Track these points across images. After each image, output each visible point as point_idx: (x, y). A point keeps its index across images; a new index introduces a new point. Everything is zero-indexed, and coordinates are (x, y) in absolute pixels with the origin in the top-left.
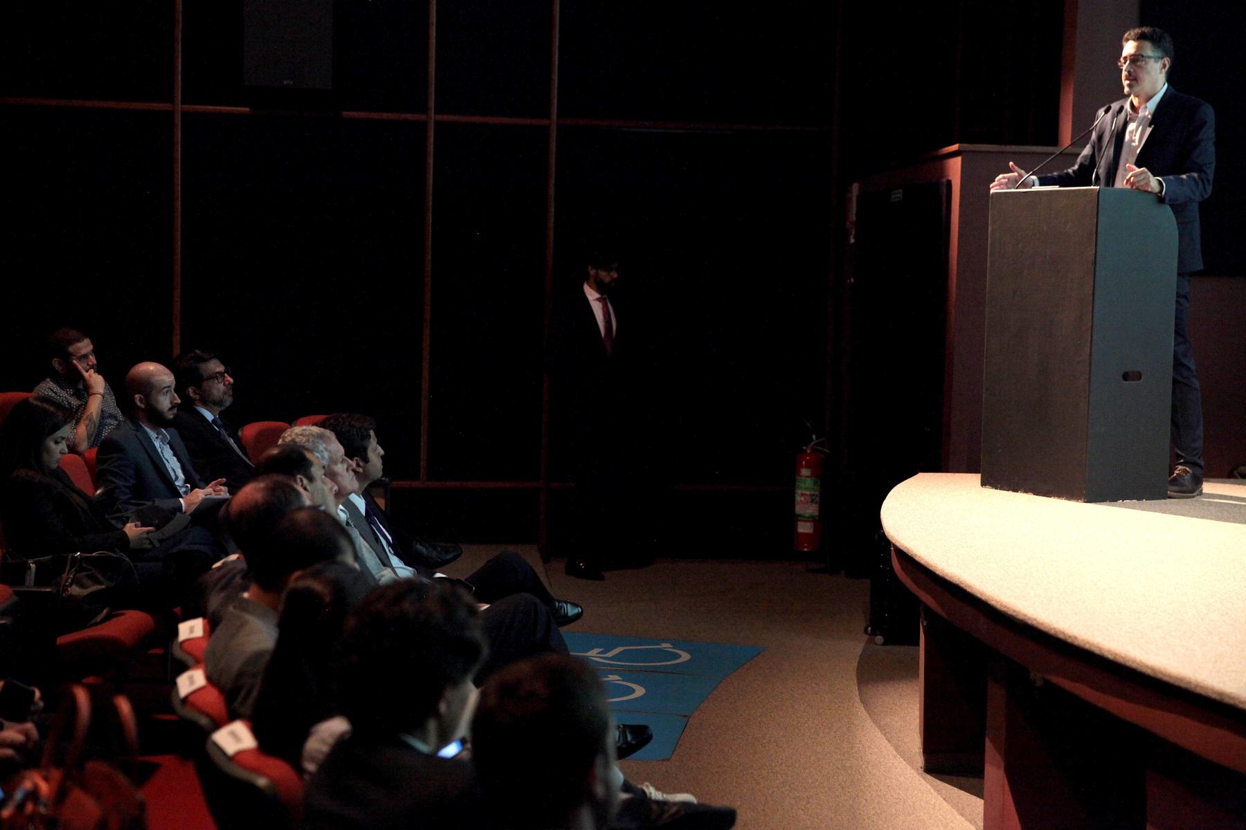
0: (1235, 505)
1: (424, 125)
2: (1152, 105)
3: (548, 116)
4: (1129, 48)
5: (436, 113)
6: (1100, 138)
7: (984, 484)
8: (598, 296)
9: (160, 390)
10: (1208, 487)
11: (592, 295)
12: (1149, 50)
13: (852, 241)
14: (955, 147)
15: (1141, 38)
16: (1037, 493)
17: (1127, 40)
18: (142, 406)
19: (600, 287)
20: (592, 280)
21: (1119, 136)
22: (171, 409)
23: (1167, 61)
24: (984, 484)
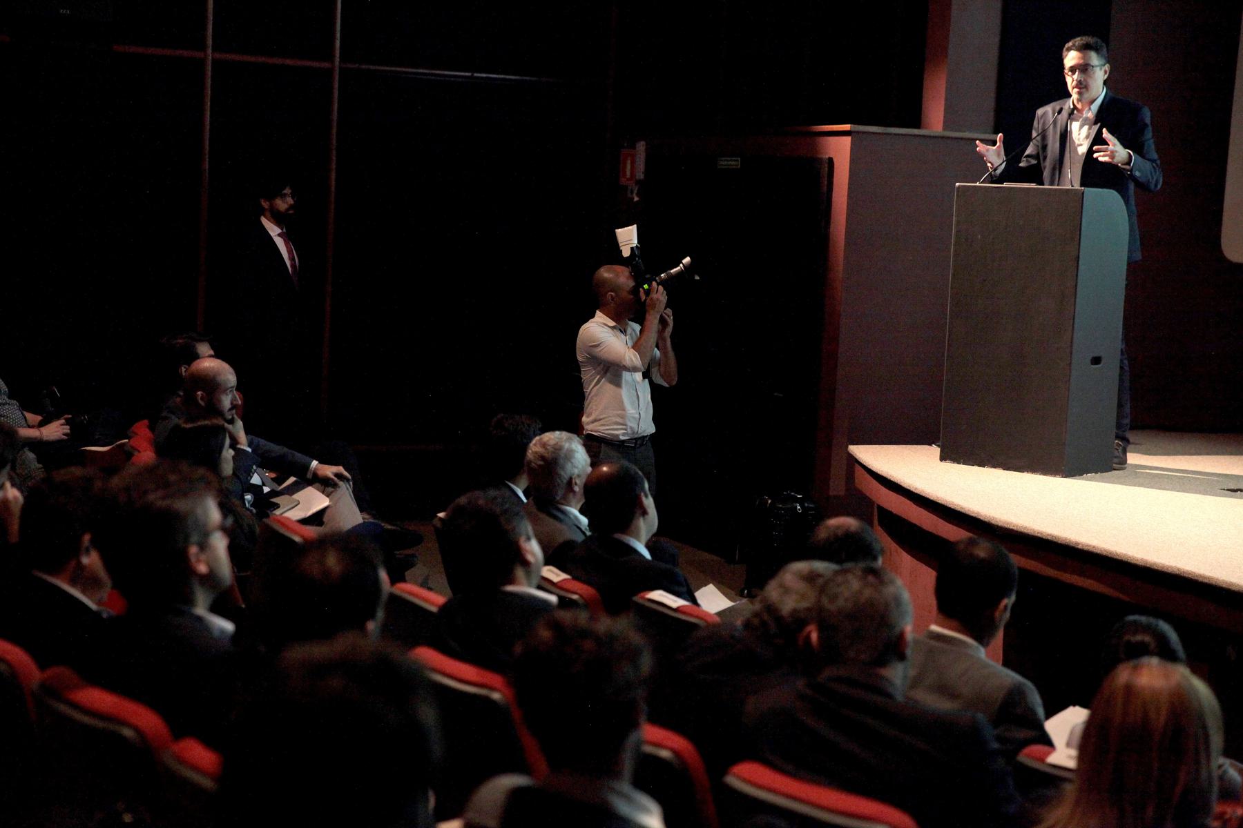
0: (1179, 478)
1: (203, 62)
2: (1095, 106)
3: (330, 58)
4: (1071, 58)
5: (214, 51)
6: (1044, 136)
7: (943, 458)
8: (279, 231)
9: (225, 391)
10: (1133, 458)
11: (274, 231)
12: (1095, 59)
13: (636, 199)
14: (847, 127)
15: (1084, 48)
16: (1007, 467)
17: (1069, 49)
18: (202, 403)
19: (278, 219)
20: (268, 214)
21: (1065, 136)
22: (230, 410)
23: (1107, 67)
24: (943, 458)
